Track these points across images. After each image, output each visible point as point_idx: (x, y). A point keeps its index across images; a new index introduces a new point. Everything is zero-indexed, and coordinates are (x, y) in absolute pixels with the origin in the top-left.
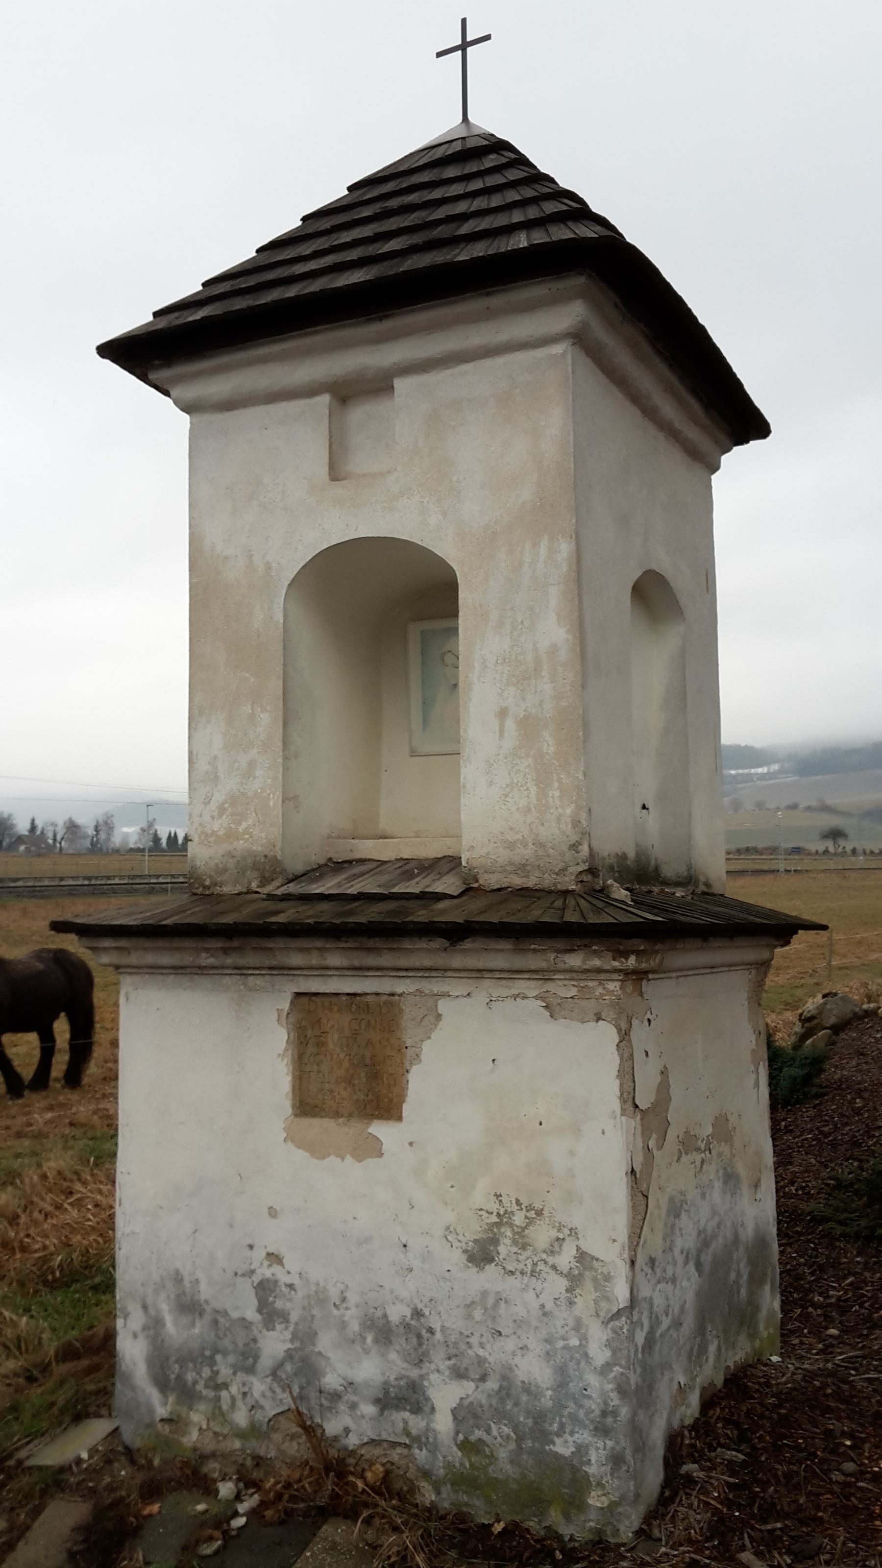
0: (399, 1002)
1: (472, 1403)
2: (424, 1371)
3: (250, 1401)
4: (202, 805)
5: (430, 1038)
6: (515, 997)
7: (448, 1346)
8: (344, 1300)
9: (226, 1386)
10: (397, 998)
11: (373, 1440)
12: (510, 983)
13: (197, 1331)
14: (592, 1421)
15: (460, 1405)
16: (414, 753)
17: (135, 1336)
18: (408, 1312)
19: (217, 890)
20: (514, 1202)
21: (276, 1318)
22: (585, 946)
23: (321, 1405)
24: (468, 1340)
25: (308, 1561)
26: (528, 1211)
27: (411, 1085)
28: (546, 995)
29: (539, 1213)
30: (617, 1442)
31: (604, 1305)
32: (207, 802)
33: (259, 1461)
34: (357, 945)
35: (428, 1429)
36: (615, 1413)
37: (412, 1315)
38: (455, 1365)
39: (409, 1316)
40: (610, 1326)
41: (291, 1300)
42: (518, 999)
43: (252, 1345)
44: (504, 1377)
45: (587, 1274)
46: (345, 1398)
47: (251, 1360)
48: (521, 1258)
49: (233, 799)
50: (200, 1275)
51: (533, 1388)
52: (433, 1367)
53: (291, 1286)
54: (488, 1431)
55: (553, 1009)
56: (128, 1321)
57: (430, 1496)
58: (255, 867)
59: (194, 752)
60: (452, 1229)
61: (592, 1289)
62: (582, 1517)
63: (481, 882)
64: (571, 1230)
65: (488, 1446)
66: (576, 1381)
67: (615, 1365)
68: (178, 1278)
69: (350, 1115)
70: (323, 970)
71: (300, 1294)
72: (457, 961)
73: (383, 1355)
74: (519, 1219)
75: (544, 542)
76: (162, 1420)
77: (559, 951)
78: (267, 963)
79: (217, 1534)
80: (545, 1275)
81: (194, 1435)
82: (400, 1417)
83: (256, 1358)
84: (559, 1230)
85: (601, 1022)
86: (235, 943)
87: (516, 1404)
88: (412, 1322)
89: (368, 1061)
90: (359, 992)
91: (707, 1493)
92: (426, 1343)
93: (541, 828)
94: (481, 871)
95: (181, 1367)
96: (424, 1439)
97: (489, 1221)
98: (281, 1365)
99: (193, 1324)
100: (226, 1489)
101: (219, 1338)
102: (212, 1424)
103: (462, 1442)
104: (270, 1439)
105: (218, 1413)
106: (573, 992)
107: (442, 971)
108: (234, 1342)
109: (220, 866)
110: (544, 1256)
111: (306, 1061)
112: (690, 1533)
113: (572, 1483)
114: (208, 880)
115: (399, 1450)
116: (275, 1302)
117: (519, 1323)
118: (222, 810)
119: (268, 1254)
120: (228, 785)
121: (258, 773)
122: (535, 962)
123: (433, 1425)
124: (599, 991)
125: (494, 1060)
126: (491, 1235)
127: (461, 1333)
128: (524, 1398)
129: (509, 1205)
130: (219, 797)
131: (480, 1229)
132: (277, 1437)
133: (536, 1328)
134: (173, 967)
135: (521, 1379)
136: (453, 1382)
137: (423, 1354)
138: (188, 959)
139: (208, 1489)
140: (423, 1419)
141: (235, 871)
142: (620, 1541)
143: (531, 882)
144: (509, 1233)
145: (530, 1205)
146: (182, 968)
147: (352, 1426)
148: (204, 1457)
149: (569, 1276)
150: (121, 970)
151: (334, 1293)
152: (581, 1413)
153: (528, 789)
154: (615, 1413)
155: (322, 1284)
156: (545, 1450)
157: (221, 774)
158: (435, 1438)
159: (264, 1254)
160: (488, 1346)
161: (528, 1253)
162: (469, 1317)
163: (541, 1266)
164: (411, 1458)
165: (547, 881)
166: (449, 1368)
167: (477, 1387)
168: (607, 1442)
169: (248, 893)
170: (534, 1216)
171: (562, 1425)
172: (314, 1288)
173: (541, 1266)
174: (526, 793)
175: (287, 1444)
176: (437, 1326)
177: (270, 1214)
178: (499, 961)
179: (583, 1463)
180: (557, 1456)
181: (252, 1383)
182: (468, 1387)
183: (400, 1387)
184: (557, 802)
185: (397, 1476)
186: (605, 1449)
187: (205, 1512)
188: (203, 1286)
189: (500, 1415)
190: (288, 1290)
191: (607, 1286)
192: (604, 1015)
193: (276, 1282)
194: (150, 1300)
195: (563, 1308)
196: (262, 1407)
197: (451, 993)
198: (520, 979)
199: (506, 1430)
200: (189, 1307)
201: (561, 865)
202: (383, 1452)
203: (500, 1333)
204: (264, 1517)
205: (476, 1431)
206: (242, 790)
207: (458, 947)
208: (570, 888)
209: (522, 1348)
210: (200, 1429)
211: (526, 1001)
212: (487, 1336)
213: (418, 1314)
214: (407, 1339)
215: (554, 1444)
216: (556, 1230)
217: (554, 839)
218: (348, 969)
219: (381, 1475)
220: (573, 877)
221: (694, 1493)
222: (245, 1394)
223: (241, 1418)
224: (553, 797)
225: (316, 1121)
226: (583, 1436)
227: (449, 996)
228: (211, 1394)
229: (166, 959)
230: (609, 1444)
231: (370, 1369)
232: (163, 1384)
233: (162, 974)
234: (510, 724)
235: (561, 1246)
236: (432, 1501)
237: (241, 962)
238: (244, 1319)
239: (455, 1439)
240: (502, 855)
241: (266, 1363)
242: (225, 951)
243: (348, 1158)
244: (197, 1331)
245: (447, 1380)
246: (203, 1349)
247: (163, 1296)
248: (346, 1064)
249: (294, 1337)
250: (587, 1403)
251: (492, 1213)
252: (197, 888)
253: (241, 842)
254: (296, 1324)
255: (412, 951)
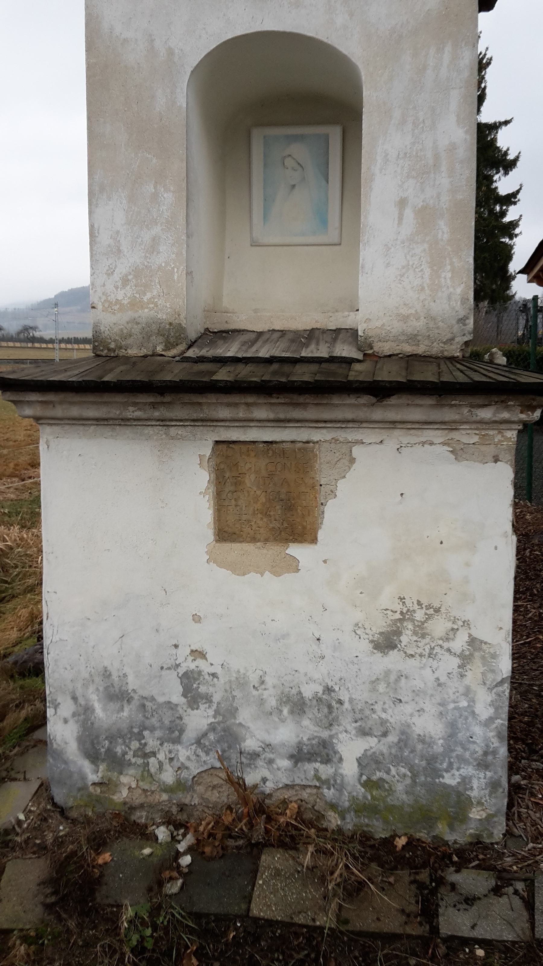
0: (314, 448)
1: (374, 753)
2: (334, 732)
3: (176, 764)
4: (105, 276)
5: (344, 477)
6: (423, 443)
7: (354, 712)
8: (263, 682)
9: (154, 754)
10: (311, 444)
11: (287, 785)
12: (419, 432)
13: (125, 714)
14: (476, 759)
15: (365, 755)
16: (255, 244)
17: (66, 721)
18: (320, 689)
19: (122, 352)
20: (415, 603)
21: (199, 700)
22: (502, 402)
23: (241, 763)
24: (372, 707)
25: (263, 888)
26: (427, 609)
27: (326, 515)
28: (450, 442)
29: (437, 611)
30: (495, 773)
31: (490, 676)
32: (110, 273)
33: (182, 807)
34: (287, 400)
35: (335, 774)
36: (494, 752)
37: (324, 691)
38: (361, 726)
39: (321, 692)
40: (494, 690)
41: (214, 686)
42: (425, 445)
43: (178, 721)
44: (403, 733)
45: (477, 654)
46: (263, 757)
47: (177, 733)
48: (420, 644)
49: (137, 272)
50: (127, 670)
51: (427, 739)
52: (341, 728)
53: (214, 675)
54: (388, 772)
55: (459, 453)
56: (58, 710)
57: (337, 821)
58: (160, 333)
59: (96, 226)
60: (360, 625)
61: (481, 665)
62: (464, 827)
63: (376, 349)
64: (464, 622)
65: (387, 783)
66: (464, 732)
67: (497, 719)
68: (106, 674)
69: (266, 540)
70: (246, 422)
71: (222, 680)
72: (378, 414)
73: (298, 723)
74: (419, 615)
75: (448, 48)
76: (94, 784)
77: (472, 406)
78: (195, 416)
79: (175, 874)
80: (440, 656)
81: (125, 793)
82: (310, 768)
83: (182, 731)
84: (454, 623)
85: (499, 463)
86: (167, 398)
87: (412, 751)
88: (324, 697)
89: (283, 496)
90: (278, 440)
91: (535, 796)
92: (336, 710)
93: (432, 304)
94: (376, 340)
95: (111, 743)
96: (332, 782)
97: (393, 618)
98: (205, 735)
99: (122, 709)
100: (162, 833)
101: (147, 718)
102: (141, 783)
103: (365, 782)
104: (194, 791)
105: (146, 774)
106: (476, 439)
107: (357, 423)
108: (161, 721)
109: (125, 331)
110: (441, 642)
111: (224, 496)
112: (538, 828)
113: (458, 804)
114: (113, 343)
115: (308, 790)
116: (199, 687)
117: (416, 693)
118: (125, 281)
119: (192, 651)
120: (131, 259)
121: (162, 248)
122: (449, 415)
123: (341, 771)
124: (499, 437)
125: (402, 494)
126: (395, 629)
127: (366, 702)
128: (419, 747)
129: (411, 605)
130: (122, 269)
131: (385, 624)
132: (200, 789)
133: (432, 695)
134: (97, 420)
135: (418, 733)
136: (359, 739)
137: (333, 720)
138: (115, 412)
139: (146, 835)
140: (332, 767)
141: (140, 336)
142: (494, 841)
143: (421, 350)
144: (410, 626)
145: (430, 605)
146: (106, 420)
147: (270, 777)
148: (132, 808)
149: (462, 656)
150: (40, 422)
151: (254, 679)
152: (467, 755)
153: (422, 270)
154: (494, 752)
155: (242, 671)
156: (435, 782)
157: (124, 248)
158: (342, 780)
159: (189, 651)
160: (390, 711)
161: (427, 640)
162: (374, 690)
163: (437, 650)
164: (320, 796)
165: (436, 349)
166: (355, 728)
167: (379, 742)
168: (487, 773)
169: (153, 355)
170: (433, 613)
171: (451, 765)
172: (235, 675)
173: (437, 650)
174: (420, 274)
175: (209, 793)
176: (345, 697)
177: (193, 620)
178: (416, 414)
179: (466, 789)
180: (445, 786)
181: (178, 751)
182: (372, 742)
183: (312, 746)
184: (448, 281)
185: (306, 809)
186: (485, 778)
187: (151, 854)
188: (131, 679)
189: (398, 760)
190: (211, 677)
191: (492, 662)
192: (501, 457)
193: (200, 673)
194: (78, 694)
195: (456, 679)
196: (187, 768)
197: (364, 441)
198: (427, 429)
199: (403, 770)
200: (117, 695)
201: (449, 336)
202: (295, 793)
203: (400, 701)
204: (204, 853)
205: (378, 773)
206: (146, 263)
207: (385, 403)
208: (455, 355)
209: (418, 711)
210: (130, 788)
211: (433, 446)
212: (389, 703)
213: (329, 690)
214: (319, 710)
215: (443, 777)
216: (451, 622)
217: (444, 314)
218: (269, 421)
219: (296, 810)
220: (459, 346)
221: (526, 797)
222: (171, 759)
223: (168, 777)
224: (445, 278)
225: (236, 546)
226: (468, 770)
227: (363, 443)
228: (140, 761)
229: (92, 412)
230: (489, 774)
231: (287, 733)
232: (94, 757)
233: (83, 425)
234: (409, 213)
235: (454, 635)
236: (338, 825)
237: (168, 414)
238: (169, 702)
239: (359, 780)
240: (397, 327)
241: (190, 734)
242: (154, 406)
243: (267, 574)
244: (125, 714)
245: (354, 738)
246: (132, 727)
247: (91, 689)
248: (263, 499)
249: (217, 713)
250: (472, 747)
251: (396, 612)
252: (102, 351)
253: (146, 310)
254: (219, 703)
255: (337, 406)
